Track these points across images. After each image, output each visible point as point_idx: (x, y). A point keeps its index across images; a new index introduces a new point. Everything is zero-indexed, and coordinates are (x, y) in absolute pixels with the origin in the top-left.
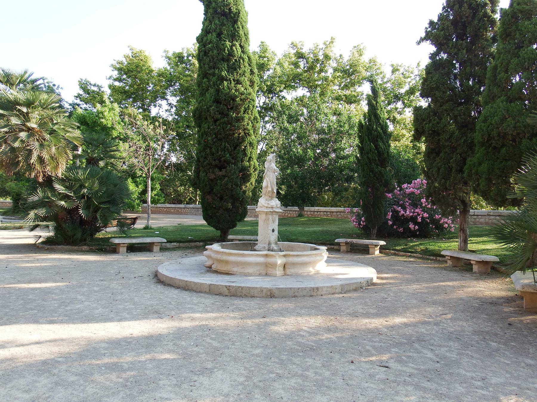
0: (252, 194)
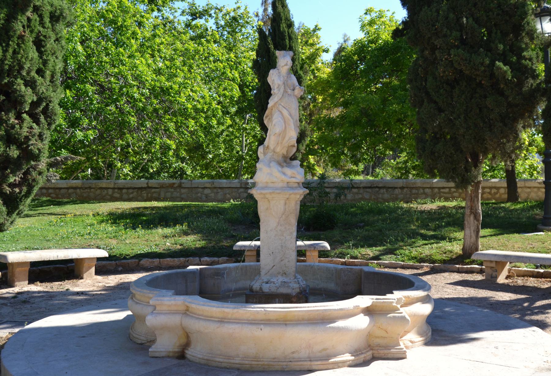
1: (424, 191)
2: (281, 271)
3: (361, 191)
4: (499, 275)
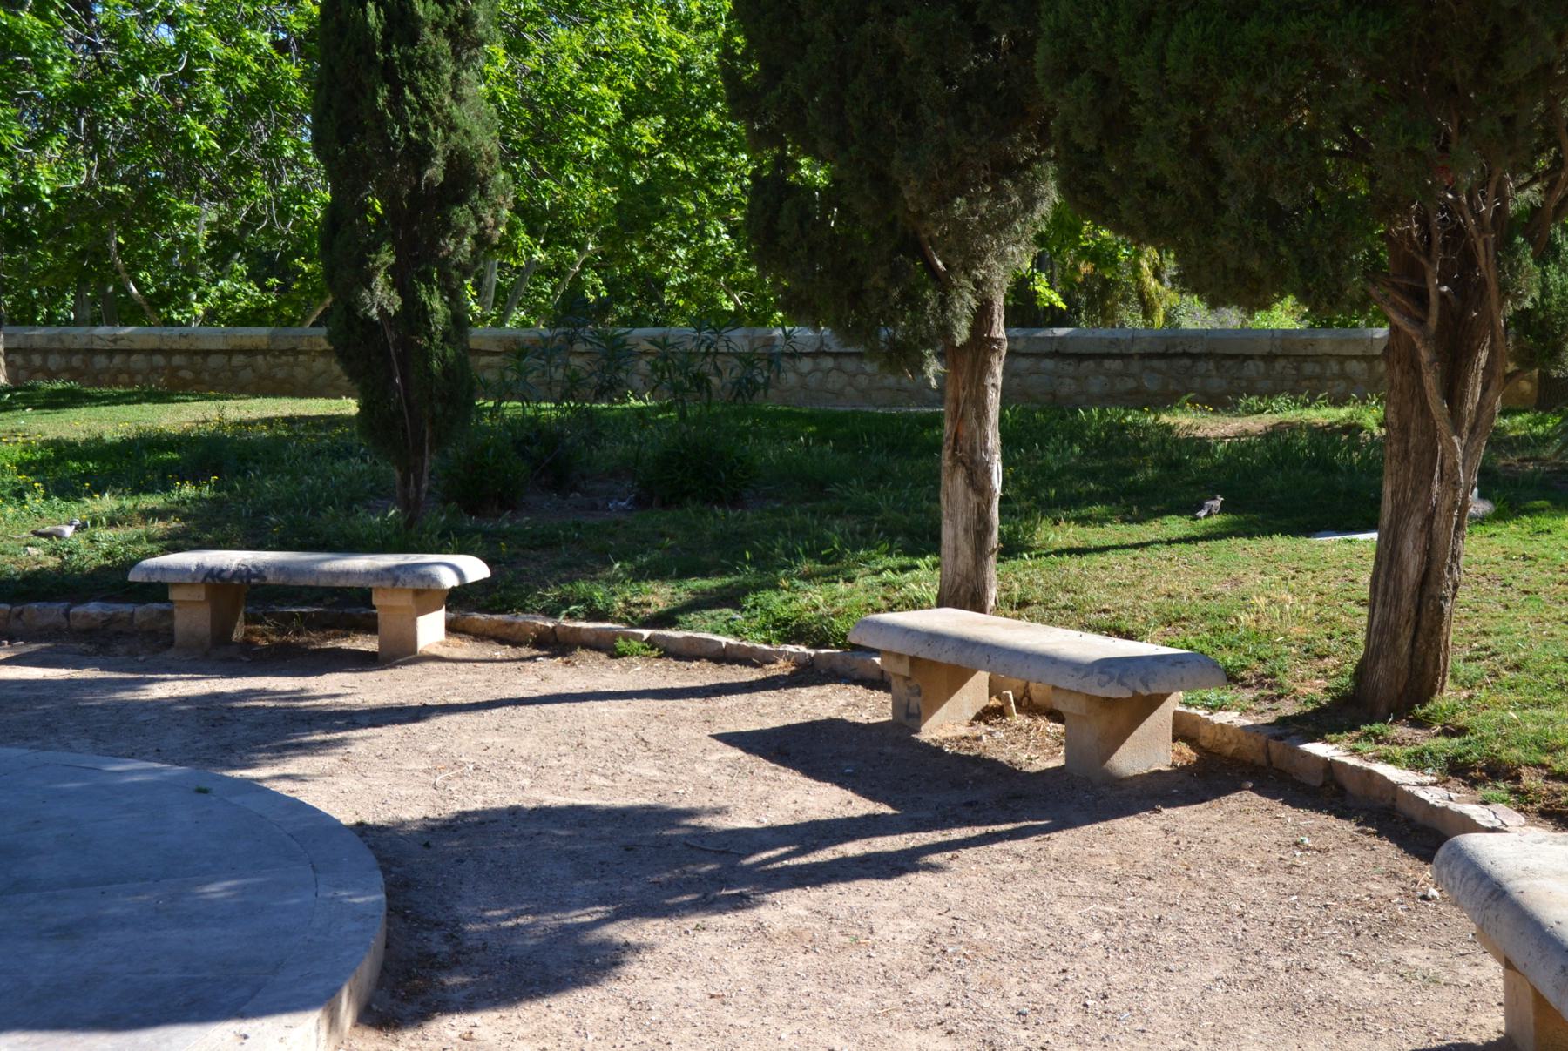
0: (810, 425)
1: (1342, 370)
3: (1135, 366)
4: (931, 712)
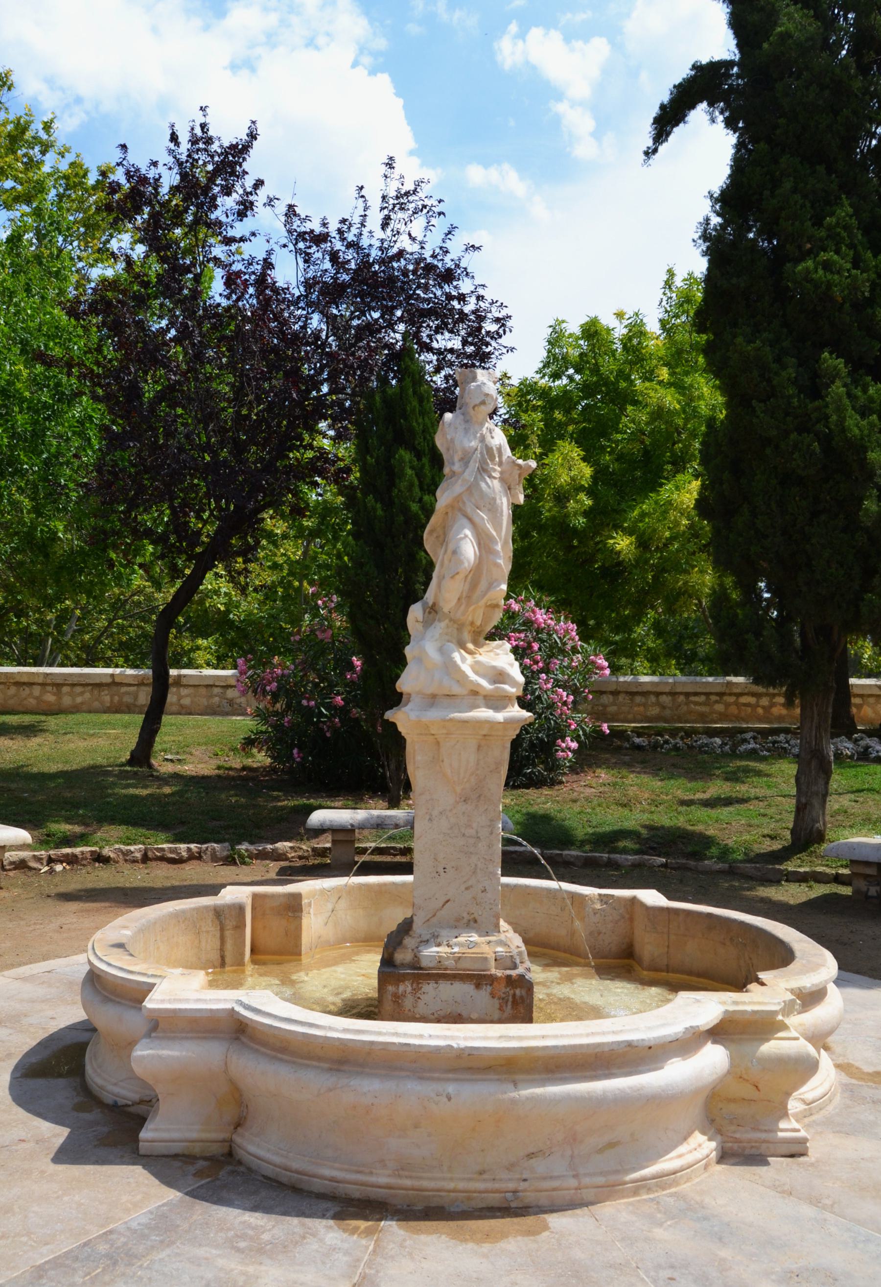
2: (465, 915)
